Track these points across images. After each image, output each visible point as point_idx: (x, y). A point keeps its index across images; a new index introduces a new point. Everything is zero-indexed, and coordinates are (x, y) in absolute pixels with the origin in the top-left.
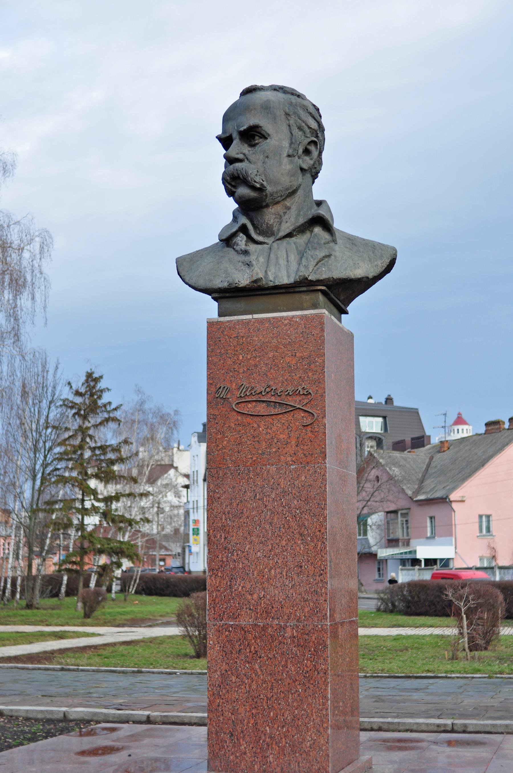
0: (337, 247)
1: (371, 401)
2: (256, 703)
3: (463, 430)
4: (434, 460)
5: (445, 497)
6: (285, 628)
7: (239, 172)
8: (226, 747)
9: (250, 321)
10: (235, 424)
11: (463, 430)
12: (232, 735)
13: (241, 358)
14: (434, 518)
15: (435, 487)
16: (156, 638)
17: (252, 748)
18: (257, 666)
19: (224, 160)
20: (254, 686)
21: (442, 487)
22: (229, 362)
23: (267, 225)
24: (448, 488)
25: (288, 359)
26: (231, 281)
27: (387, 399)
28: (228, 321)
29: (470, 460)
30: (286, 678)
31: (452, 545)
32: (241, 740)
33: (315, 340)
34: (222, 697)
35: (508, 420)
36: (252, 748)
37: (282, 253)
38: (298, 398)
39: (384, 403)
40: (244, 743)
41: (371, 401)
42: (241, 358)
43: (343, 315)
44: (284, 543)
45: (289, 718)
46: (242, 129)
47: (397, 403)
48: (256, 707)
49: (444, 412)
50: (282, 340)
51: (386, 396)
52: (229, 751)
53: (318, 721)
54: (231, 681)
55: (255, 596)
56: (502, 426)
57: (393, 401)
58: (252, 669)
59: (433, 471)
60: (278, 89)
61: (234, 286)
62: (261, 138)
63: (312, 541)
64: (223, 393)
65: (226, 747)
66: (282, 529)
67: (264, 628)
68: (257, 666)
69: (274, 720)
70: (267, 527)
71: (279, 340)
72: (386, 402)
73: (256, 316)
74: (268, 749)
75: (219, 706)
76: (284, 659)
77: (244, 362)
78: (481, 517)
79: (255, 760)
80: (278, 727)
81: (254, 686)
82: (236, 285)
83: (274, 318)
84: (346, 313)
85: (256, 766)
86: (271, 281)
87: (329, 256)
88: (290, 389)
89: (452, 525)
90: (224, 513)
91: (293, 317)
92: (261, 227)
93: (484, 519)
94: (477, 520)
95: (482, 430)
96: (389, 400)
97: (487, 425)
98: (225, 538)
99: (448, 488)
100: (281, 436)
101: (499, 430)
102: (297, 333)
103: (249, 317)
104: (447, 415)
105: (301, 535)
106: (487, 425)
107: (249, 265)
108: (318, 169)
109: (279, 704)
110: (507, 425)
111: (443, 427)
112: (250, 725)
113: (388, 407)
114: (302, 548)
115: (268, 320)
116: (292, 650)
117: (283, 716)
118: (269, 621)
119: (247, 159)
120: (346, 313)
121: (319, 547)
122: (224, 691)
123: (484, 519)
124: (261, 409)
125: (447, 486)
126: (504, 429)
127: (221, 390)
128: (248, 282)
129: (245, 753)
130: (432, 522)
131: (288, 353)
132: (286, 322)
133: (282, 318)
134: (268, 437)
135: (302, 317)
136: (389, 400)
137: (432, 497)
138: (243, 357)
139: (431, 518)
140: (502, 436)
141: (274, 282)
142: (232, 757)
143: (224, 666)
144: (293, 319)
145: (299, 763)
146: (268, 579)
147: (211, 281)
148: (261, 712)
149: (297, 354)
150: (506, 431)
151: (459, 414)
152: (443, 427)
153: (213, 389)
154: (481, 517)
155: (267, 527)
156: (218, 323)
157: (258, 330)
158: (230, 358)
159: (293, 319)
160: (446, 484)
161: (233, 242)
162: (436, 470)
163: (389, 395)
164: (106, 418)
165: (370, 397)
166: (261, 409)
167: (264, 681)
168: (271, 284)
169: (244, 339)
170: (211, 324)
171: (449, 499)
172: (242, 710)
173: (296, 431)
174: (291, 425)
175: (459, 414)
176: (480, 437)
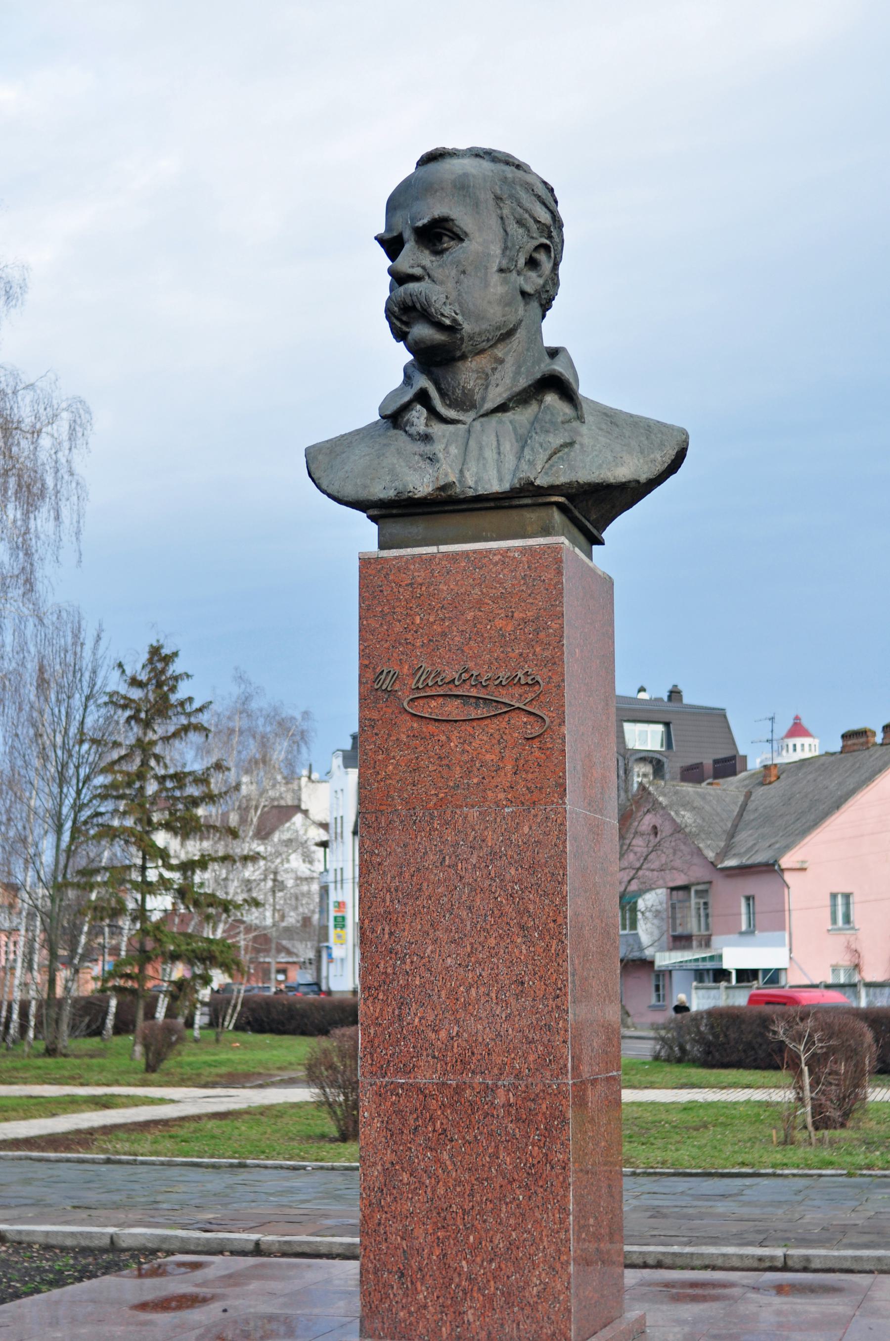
0: (584, 429)
1: (643, 696)
2: (445, 1219)
3: (803, 745)
4: (752, 798)
5: (771, 862)
6: (494, 1089)
7: (415, 299)
8: (392, 1296)
9: (433, 556)
10: (408, 736)
11: (803, 745)
12: (402, 1275)
13: (418, 621)
14: (753, 898)
15: (755, 844)
16: (270, 1107)
17: (438, 1297)
18: (445, 1156)
19: (389, 278)
20: (441, 1191)
21: (768, 845)
22: (398, 627)
23: (463, 391)
24: (777, 846)
25: (499, 623)
26: (401, 488)
27: (671, 692)
28: (396, 558)
29: (816, 797)
30: (496, 1177)
31: (784, 945)
32: (419, 1284)
33: (547, 590)
34: (386, 1209)
35: (881, 729)
36: (438, 1297)
37: (490, 439)
38: (517, 691)
39: (666, 699)
40: (423, 1288)
41: (643, 696)
42: (418, 621)
43: (595, 547)
44: (492, 942)
45: (501, 1245)
46: (420, 224)
47: (687, 699)
48: (443, 1227)
49: (771, 715)
50: (490, 591)
51: (670, 687)
52: (397, 1302)
53: (551, 1250)
54: (401, 1181)
55: (443, 1034)
56: (871, 740)
57: (681, 696)
58: (438, 1160)
59: (752, 817)
60: (482, 154)
61: (405, 496)
62: (453, 239)
63: (541, 937)
64: (387, 682)
65: (392, 1296)
66: (489, 918)
67: (458, 1090)
68: (445, 1156)
69: (475, 1248)
70: (464, 914)
71: (484, 590)
72: (670, 698)
73: (444, 548)
74: (465, 1299)
75: (379, 1224)
76: (493, 1144)
77: (422, 629)
78: (834, 896)
79: (442, 1319)
80: (482, 1262)
81: (441, 1191)
82: (410, 494)
83: (475, 552)
84: (601, 542)
85: (444, 1329)
86: (470, 488)
87: (571, 444)
88: (503, 674)
89: (784, 911)
90: (389, 891)
91: (508, 550)
92: (453, 394)
93: (840, 900)
94: (827, 901)
95: (837, 745)
96: (675, 694)
97: (845, 737)
98: (391, 934)
99: (777, 846)
100: (489, 757)
101: (866, 746)
102: (515, 577)
103: (432, 549)
104: (776, 720)
105: (522, 928)
106: (845, 737)
107: (432, 459)
108: (551, 293)
109: (485, 1221)
110: (879, 738)
111: (769, 741)
112: (434, 1257)
113: (673, 706)
114: (524, 951)
115: (466, 554)
116: (506, 1127)
117: (491, 1241)
118: (467, 1077)
119: (429, 276)
120: (601, 542)
121: (553, 948)
122: (388, 1199)
123: (840, 900)
124: (453, 709)
125: (777, 842)
126: (875, 744)
127: (383, 677)
128: (430, 489)
129: (425, 1307)
130: (749, 905)
131: (500, 611)
132: (497, 558)
133: (489, 551)
134: (465, 757)
135: (524, 550)
136: (675, 694)
137: (749, 862)
138: (421, 619)
139: (748, 898)
140: (871, 756)
141: (476, 490)
142: (402, 1314)
143: (389, 1156)
144: (509, 554)
145: (518, 1324)
146: (465, 1005)
147: (365, 487)
148: (453, 1236)
149: (515, 615)
150: (878, 747)
151: (797, 718)
152: (769, 741)
153: (370, 675)
154: (834, 896)
155: (464, 914)
156: (377, 559)
157: (448, 573)
158: (400, 621)
159: (509, 554)
160: (773, 840)
161: (405, 419)
162: (756, 815)
163: (675, 686)
164: (184, 725)
165: (642, 690)
166: (453, 709)
167: (459, 1182)
168: (471, 493)
169: (424, 588)
170: (366, 563)
171: (779, 866)
172: (419, 1232)
173: (513, 748)
174: (505, 737)
175: (797, 718)
176: (833, 758)
